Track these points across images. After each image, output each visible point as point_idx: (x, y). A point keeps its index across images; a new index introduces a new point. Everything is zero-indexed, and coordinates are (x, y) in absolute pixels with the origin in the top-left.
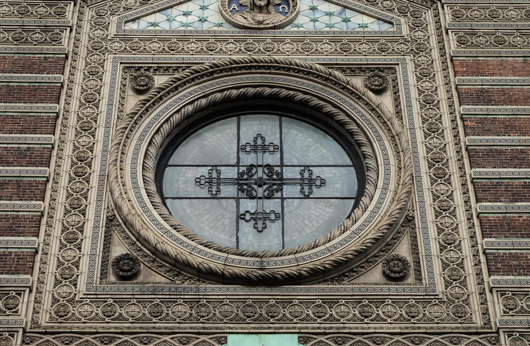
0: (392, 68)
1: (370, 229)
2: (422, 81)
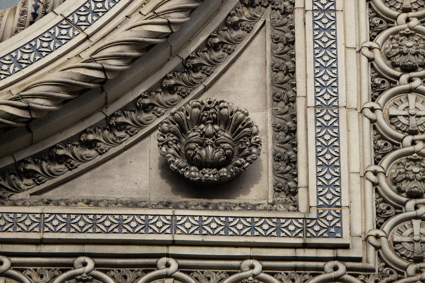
1: (126, 12)
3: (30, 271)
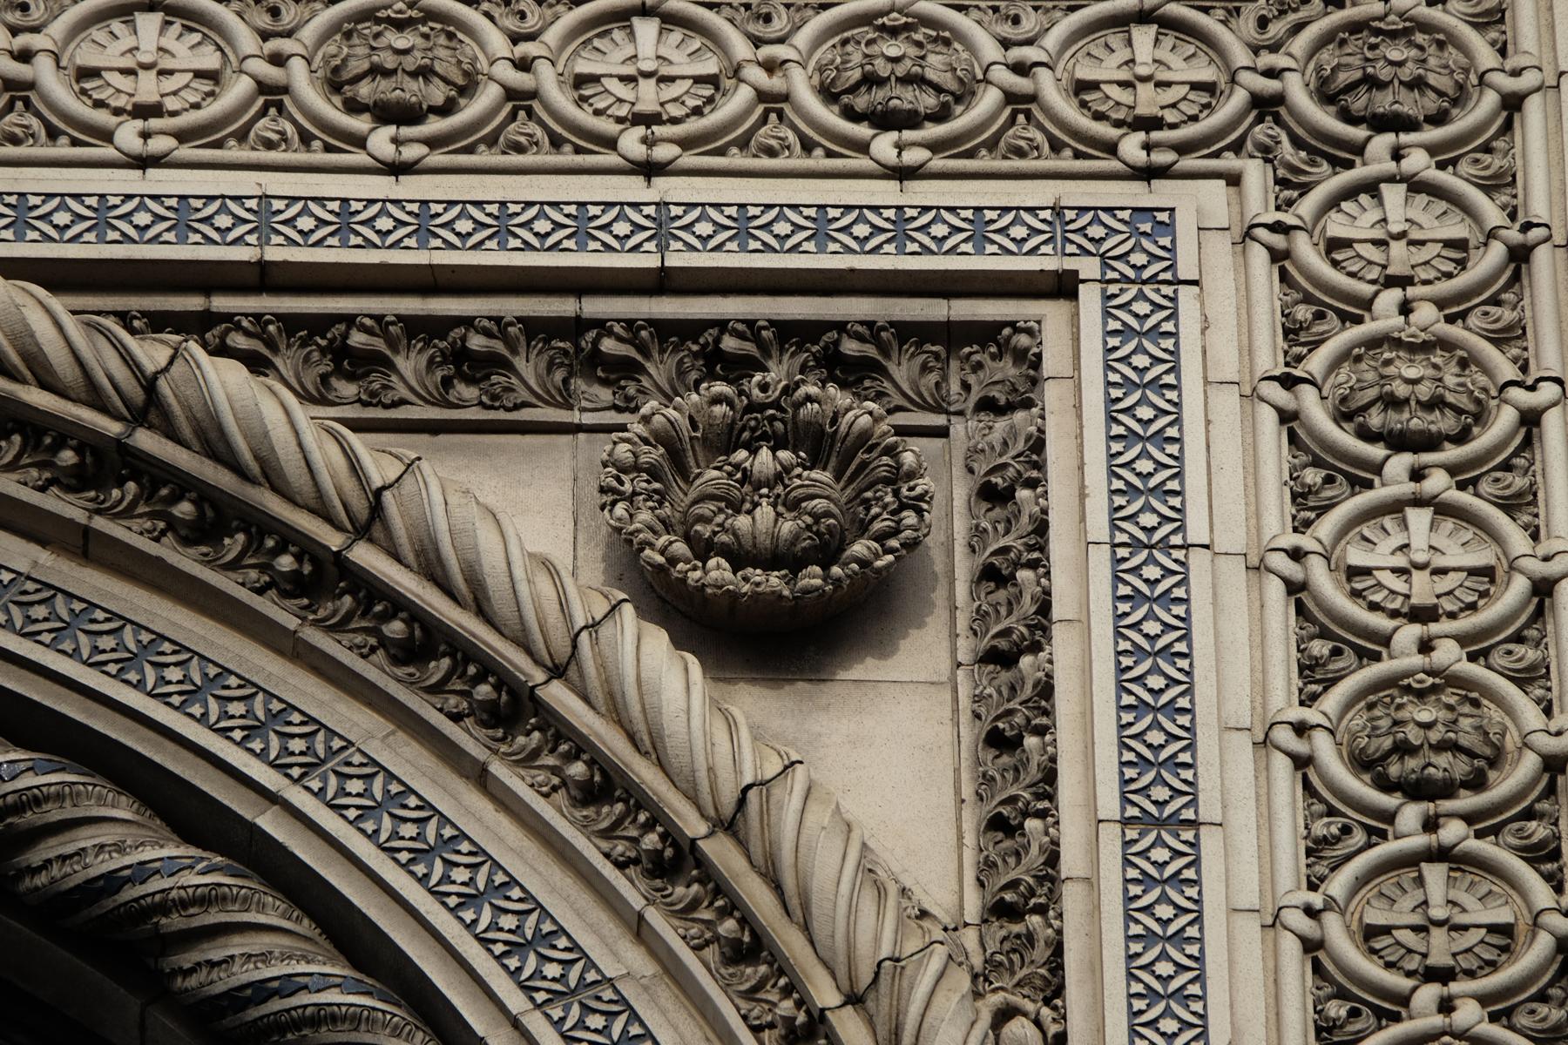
0: (986, 333)
2: (1365, 499)
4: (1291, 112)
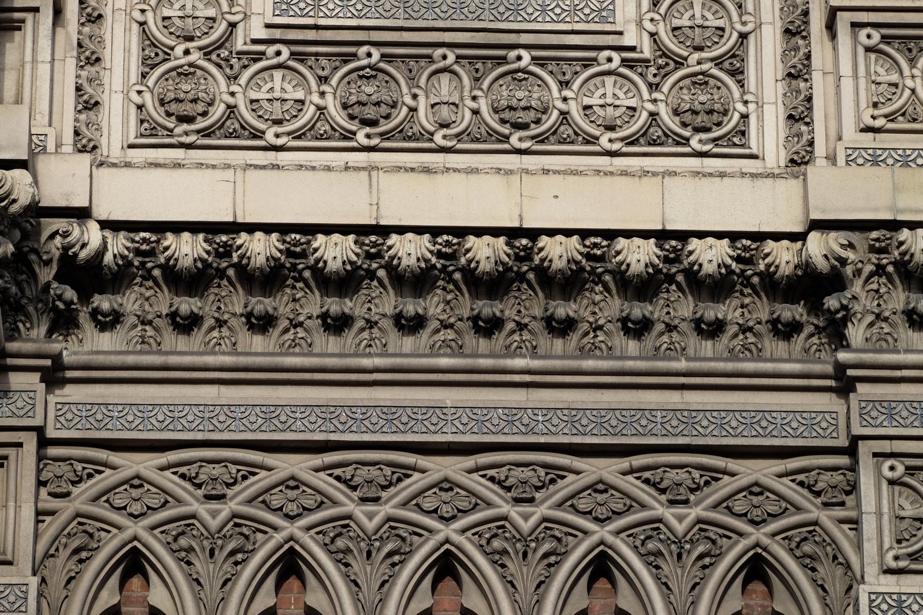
3: (311, 61)
4: (328, 113)
